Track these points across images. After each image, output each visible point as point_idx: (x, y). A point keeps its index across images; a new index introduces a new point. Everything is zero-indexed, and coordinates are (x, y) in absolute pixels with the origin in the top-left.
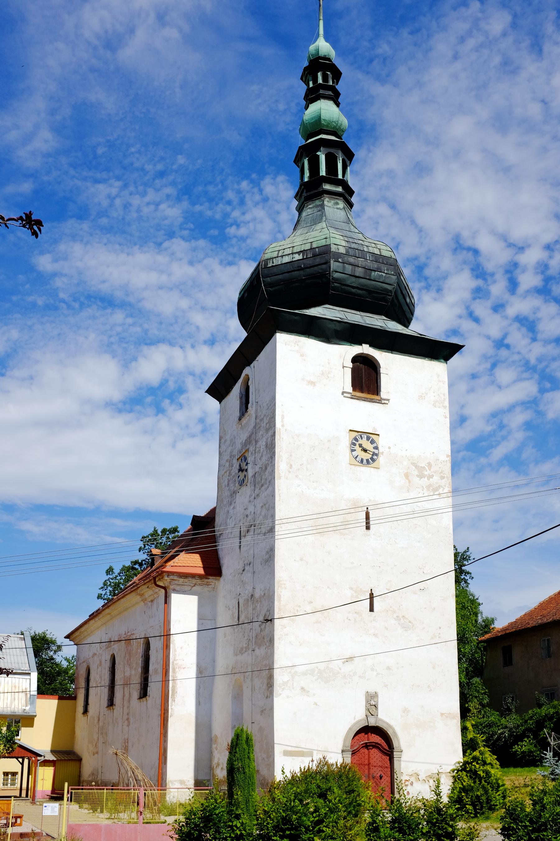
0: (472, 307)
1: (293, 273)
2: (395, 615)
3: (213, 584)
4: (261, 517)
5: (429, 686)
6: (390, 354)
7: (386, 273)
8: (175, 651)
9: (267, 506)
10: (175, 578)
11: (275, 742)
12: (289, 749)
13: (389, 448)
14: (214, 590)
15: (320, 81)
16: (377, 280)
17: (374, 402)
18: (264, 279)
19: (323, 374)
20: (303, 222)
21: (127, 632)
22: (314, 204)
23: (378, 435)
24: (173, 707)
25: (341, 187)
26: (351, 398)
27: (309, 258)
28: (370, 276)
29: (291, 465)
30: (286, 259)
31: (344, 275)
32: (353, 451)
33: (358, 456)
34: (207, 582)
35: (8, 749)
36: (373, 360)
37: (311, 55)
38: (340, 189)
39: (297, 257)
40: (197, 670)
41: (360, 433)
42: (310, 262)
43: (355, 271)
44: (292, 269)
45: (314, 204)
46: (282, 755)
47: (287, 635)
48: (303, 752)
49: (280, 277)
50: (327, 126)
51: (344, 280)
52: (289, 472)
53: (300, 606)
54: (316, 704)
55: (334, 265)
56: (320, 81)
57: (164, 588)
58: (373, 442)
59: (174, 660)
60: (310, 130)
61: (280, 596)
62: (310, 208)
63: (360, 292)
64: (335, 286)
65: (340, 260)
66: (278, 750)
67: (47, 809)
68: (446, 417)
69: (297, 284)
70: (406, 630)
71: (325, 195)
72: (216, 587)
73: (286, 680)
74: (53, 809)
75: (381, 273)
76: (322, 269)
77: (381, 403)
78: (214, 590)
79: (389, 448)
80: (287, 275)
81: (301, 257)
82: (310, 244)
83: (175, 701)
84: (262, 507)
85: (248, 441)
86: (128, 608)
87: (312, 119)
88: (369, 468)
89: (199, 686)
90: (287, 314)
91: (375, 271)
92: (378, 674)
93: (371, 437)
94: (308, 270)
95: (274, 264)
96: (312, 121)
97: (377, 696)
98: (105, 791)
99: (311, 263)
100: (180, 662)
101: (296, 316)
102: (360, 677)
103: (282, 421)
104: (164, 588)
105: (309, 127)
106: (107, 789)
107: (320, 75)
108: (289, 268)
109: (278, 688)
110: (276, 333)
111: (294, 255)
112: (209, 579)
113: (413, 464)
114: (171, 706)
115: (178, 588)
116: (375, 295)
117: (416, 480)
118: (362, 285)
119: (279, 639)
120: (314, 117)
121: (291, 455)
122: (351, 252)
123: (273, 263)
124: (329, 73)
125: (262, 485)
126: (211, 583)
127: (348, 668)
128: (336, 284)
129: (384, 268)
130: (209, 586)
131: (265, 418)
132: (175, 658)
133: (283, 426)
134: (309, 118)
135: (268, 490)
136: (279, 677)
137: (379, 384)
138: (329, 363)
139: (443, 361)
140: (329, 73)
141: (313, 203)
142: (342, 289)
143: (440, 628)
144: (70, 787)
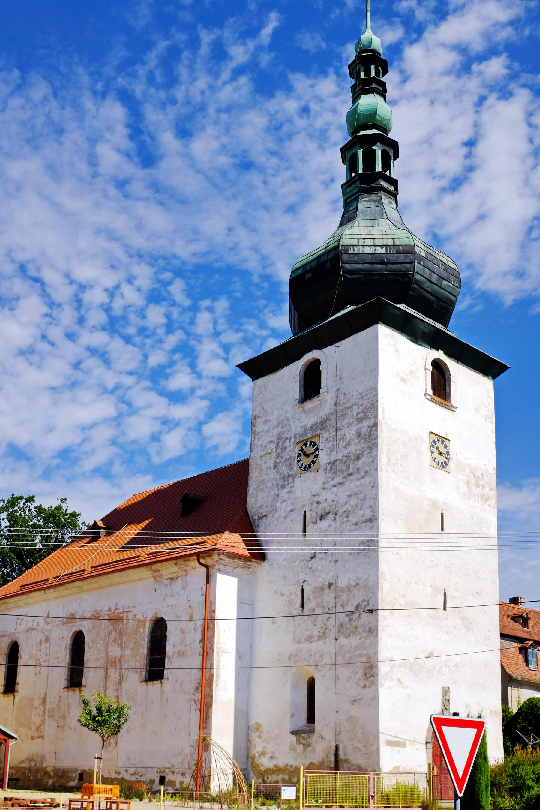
0: (81, 296)
1: (375, 265)
2: (461, 615)
3: (253, 567)
4: (348, 506)
5: (483, 685)
6: (457, 364)
7: (453, 285)
8: (219, 634)
9: (360, 496)
10: (224, 558)
11: (380, 731)
12: (390, 738)
13: (457, 454)
14: (252, 574)
15: (373, 74)
16: (446, 289)
17: (446, 408)
18: (343, 265)
19: (411, 373)
20: (361, 214)
21: (113, 609)
22: (370, 198)
23: (449, 440)
24: (217, 692)
25: (393, 187)
26: (431, 401)
27: (392, 254)
28: (441, 284)
29: (390, 459)
30: (368, 250)
31: (423, 278)
32: (433, 452)
33: (435, 458)
34: (249, 565)
35: (114, 731)
36: (444, 368)
37: (363, 45)
38: (392, 188)
39: (380, 250)
40: (236, 655)
41: (437, 436)
42: (392, 258)
43: (431, 276)
44: (375, 261)
45: (370, 198)
46: (385, 744)
47: (387, 626)
48: (399, 742)
49: (361, 266)
50: (380, 122)
51: (423, 283)
52: (389, 465)
53: (396, 599)
54: (408, 696)
55: (418, 267)
56: (373, 74)
57: (207, 567)
58: (446, 447)
59: (218, 643)
60: (362, 121)
61: (383, 587)
62: (366, 201)
63: (431, 298)
64: (414, 288)
65: (422, 263)
66: (383, 739)
67: (286, 793)
68: (493, 433)
69: (377, 277)
70: (468, 631)
71: (382, 192)
72: (255, 571)
73: (387, 671)
74: (291, 793)
75: (449, 284)
76: (406, 268)
77: (451, 410)
78: (252, 574)
79: (457, 454)
80: (368, 266)
81: (384, 251)
82: (392, 240)
83: (218, 685)
84: (350, 496)
85: (322, 424)
86: (119, 583)
87: (367, 111)
88: (443, 472)
89: (239, 672)
90: (392, 308)
91: (446, 280)
92: (450, 670)
93: (445, 440)
94: (391, 265)
95: (355, 252)
96: (366, 113)
97: (450, 691)
98: (338, 775)
99: (395, 259)
100: (223, 646)
101: (398, 311)
102: (438, 672)
103: (383, 414)
104: (207, 567)
105: (362, 118)
106: (340, 773)
107: (373, 67)
108: (369, 259)
109: (382, 678)
110: (378, 323)
111: (376, 248)
112: (252, 561)
113: (472, 472)
114: (215, 691)
115: (222, 568)
116: (442, 303)
117: (474, 488)
118: (434, 292)
119: (382, 630)
120: (370, 110)
121: (389, 449)
122: (430, 257)
123: (354, 250)
124: (380, 69)
125: (351, 474)
126: (251, 566)
127: (429, 663)
128: (416, 286)
129: (452, 278)
130: (249, 570)
131: (355, 407)
132: (219, 641)
133: (384, 418)
134: (364, 109)
135: (362, 481)
136: (383, 669)
137: (447, 391)
138: (415, 363)
139: (491, 378)
140: (380, 69)
141: (368, 197)
142: (419, 291)
143: (489, 631)
144: (305, 771)
